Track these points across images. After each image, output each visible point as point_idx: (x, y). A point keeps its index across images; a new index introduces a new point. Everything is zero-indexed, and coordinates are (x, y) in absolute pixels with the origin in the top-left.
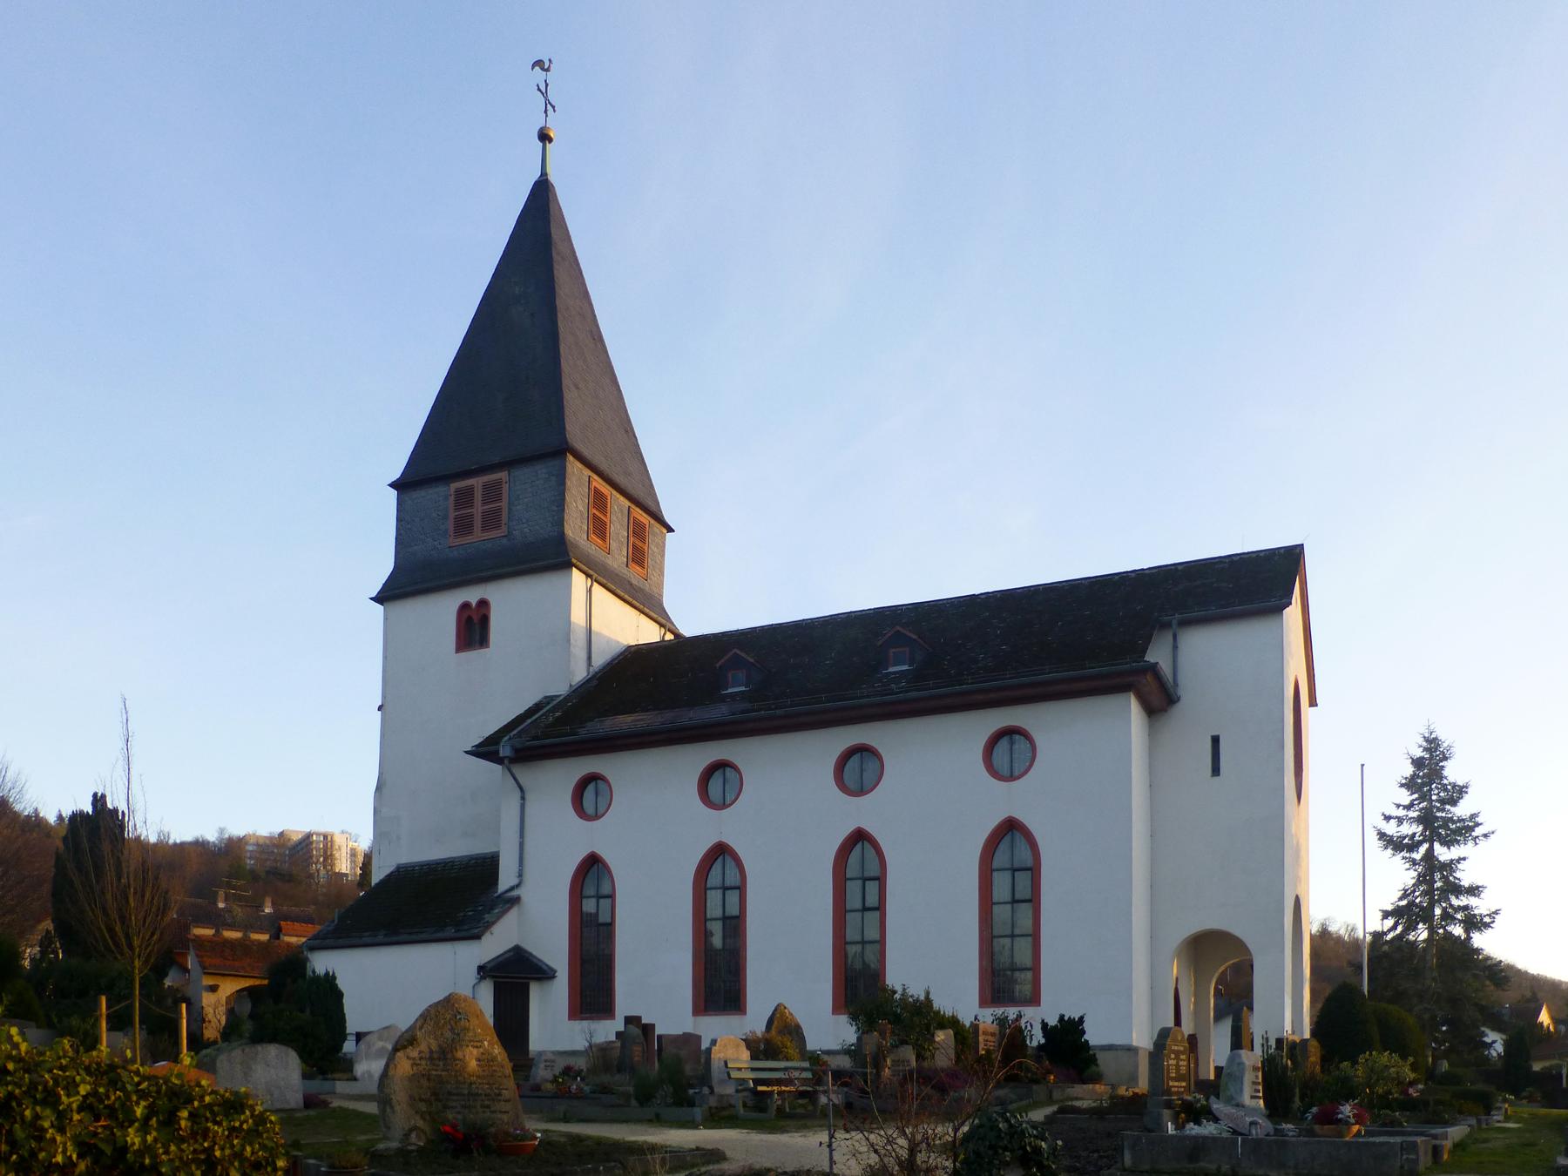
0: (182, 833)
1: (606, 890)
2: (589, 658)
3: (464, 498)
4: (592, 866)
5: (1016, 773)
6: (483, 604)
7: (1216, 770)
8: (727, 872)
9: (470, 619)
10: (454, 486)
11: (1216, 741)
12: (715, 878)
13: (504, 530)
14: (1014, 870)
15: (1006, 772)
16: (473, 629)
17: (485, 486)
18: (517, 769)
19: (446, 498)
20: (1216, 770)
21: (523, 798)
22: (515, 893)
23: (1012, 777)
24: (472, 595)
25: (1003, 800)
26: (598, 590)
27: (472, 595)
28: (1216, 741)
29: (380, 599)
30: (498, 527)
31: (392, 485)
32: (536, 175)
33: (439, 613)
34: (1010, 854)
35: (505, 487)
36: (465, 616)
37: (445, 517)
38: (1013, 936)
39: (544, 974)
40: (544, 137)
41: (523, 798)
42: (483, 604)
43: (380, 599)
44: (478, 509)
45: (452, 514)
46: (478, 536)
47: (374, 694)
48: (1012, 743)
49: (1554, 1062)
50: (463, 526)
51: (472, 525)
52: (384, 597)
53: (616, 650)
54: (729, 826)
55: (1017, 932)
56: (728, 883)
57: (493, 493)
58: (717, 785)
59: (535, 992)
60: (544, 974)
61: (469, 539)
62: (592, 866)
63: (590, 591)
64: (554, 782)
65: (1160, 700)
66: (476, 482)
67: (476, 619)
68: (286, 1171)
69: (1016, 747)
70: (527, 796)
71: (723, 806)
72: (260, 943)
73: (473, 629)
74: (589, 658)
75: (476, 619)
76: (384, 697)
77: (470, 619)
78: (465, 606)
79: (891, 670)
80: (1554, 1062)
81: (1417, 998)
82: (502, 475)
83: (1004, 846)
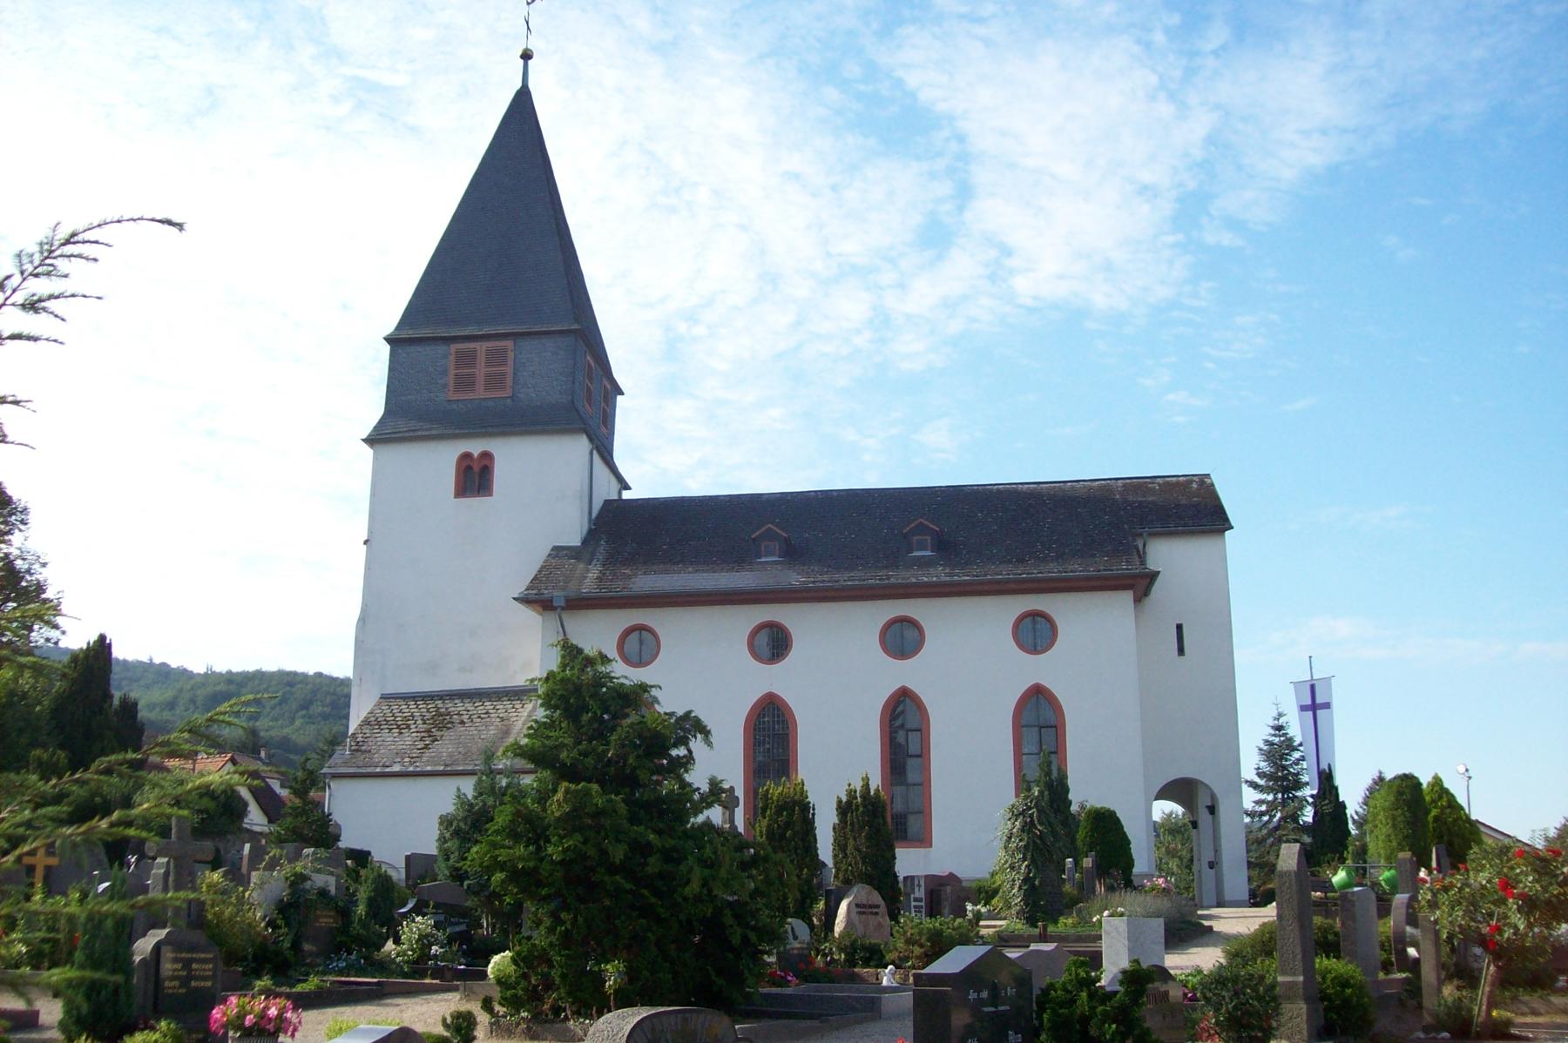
0: (130, 658)
3: (466, 359)
6: (487, 456)
7: (1181, 651)
9: (469, 468)
10: (454, 347)
11: (1179, 627)
13: (508, 392)
16: (474, 478)
17: (489, 352)
18: (565, 616)
19: (445, 356)
20: (1181, 651)
24: (476, 447)
27: (476, 447)
28: (1179, 627)
31: (388, 339)
32: (519, 85)
33: (438, 462)
34: (1039, 718)
35: (511, 355)
37: (445, 373)
40: (527, 56)
42: (487, 456)
43: (371, 441)
44: (481, 370)
45: (453, 372)
46: (480, 393)
47: (360, 528)
48: (1034, 622)
49: (144, 834)
50: (464, 383)
51: (473, 383)
54: (779, 679)
57: (497, 358)
61: (471, 396)
65: (1141, 584)
66: (481, 347)
68: (75, 1023)
73: (474, 478)
75: (476, 469)
76: (370, 531)
77: (469, 468)
78: (466, 456)
80: (144, 834)
82: (509, 344)
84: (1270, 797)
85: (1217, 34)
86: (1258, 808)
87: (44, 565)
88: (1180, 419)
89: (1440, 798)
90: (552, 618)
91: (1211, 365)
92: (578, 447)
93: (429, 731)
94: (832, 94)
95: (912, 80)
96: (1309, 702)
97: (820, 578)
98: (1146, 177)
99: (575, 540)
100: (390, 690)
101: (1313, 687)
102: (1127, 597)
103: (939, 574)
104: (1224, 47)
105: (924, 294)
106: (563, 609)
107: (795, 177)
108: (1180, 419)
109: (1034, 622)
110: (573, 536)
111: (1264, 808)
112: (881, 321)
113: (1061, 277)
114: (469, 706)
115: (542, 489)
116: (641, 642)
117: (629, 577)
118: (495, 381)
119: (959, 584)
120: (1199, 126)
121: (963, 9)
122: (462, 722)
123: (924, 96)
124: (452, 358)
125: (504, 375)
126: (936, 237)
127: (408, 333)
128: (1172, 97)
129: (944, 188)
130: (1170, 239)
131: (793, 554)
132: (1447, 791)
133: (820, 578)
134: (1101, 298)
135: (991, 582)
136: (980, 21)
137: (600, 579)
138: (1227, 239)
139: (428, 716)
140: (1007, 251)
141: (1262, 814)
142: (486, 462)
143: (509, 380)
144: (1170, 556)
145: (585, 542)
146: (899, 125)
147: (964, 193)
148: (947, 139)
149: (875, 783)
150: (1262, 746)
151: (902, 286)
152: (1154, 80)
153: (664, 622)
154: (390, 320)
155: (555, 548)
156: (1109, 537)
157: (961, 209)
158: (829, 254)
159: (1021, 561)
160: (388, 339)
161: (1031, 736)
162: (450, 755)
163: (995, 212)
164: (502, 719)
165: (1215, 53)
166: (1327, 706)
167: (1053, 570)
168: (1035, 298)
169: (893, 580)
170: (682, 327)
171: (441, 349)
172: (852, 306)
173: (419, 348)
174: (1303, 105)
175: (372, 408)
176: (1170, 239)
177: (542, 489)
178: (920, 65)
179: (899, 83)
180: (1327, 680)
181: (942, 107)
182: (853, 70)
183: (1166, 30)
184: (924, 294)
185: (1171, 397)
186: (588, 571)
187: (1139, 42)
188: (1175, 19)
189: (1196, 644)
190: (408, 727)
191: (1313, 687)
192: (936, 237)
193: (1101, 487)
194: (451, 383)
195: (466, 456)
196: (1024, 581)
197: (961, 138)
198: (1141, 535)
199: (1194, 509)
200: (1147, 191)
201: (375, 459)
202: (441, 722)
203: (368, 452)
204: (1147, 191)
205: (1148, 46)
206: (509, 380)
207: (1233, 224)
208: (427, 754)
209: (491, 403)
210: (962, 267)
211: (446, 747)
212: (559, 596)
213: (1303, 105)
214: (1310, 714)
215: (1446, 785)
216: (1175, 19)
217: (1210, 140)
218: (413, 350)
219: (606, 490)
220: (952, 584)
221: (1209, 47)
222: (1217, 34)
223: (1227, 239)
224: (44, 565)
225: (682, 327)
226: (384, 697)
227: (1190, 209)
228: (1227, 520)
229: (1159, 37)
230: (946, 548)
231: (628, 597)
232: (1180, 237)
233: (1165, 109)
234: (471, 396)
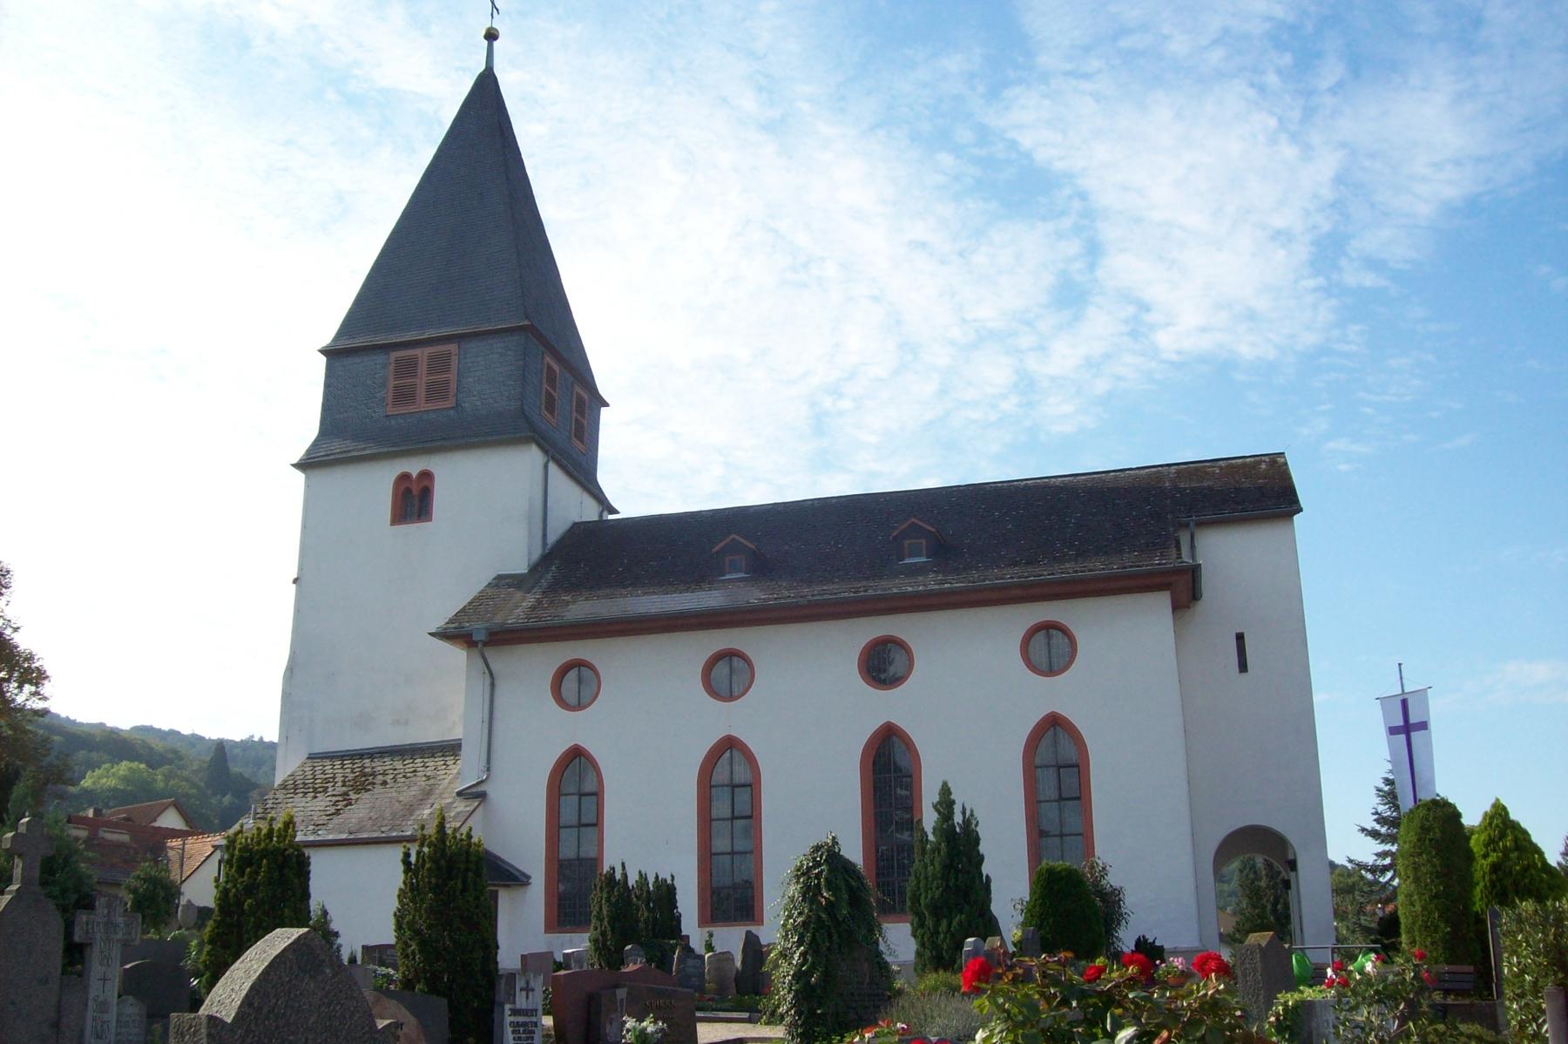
1: (589, 786)
2: (545, 535)
4: (575, 762)
5: (736, 694)
7: (1243, 667)
8: (736, 768)
9: (408, 490)
10: (394, 355)
11: (1240, 637)
12: (721, 774)
14: (1059, 767)
15: (572, 700)
16: (413, 502)
17: (431, 358)
18: (489, 652)
20: (1243, 667)
21: (493, 685)
22: (481, 789)
23: (731, 697)
24: (413, 466)
25: (1046, 695)
26: (553, 467)
27: (413, 466)
28: (1240, 637)
29: (302, 466)
30: (445, 398)
31: (324, 351)
33: (376, 484)
36: (402, 488)
38: (1061, 835)
39: (515, 879)
41: (493, 685)
42: (427, 476)
43: (302, 466)
44: (422, 380)
45: (392, 383)
46: (421, 405)
48: (1049, 637)
50: (404, 395)
52: (306, 465)
53: (567, 526)
55: (1066, 830)
56: (737, 780)
58: (726, 677)
59: (506, 902)
60: (515, 879)
61: (412, 409)
62: (575, 762)
63: (546, 467)
64: (532, 667)
65: (1184, 589)
66: (423, 353)
67: (415, 492)
69: (1054, 641)
70: (497, 682)
71: (579, 706)
72: (119, 845)
73: (413, 502)
74: (545, 535)
75: (415, 492)
76: (301, 569)
79: (907, 561)
81: (1458, 869)
82: (453, 347)
83: (1046, 741)
84: (1394, 848)
85: (1332, 71)
86: (1380, 862)
87: (16, 629)
88: (1343, 467)
89: (1502, 836)
90: (475, 652)
91: (1369, 410)
92: (525, 462)
93: (346, 794)
94: (945, 159)
95: (1026, 141)
96: (1401, 723)
97: (786, 593)
98: (1278, 222)
99: (522, 568)
100: (319, 748)
101: (1404, 703)
102: (1162, 601)
103: (931, 583)
104: (1340, 84)
105: (1065, 356)
106: (486, 644)
107: (922, 245)
108: (1343, 467)
109: (1049, 637)
110: (519, 565)
111: (1388, 861)
112: (1026, 385)
113: (1204, 330)
114: (398, 765)
115: (493, 507)
116: (580, 681)
117: (568, 603)
118: (437, 391)
119: (953, 592)
120: (1326, 165)
121: (1069, 67)
122: (385, 783)
123: (1041, 156)
124: (392, 367)
125: (447, 382)
126: (1070, 297)
127: (342, 344)
128: (1293, 138)
129: (1073, 247)
130: (1311, 283)
131: (761, 568)
132: (1515, 827)
133: (786, 593)
134: (1247, 348)
135: (993, 588)
136: (1086, 76)
137: (533, 608)
138: (1369, 280)
139: (351, 776)
140: (1145, 307)
141: (1385, 869)
142: (425, 483)
143: (453, 386)
144: (1225, 553)
145: (534, 569)
146: (1022, 189)
147: (1094, 251)
148: (1070, 197)
149: (853, 851)
150: (1382, 786)
151: (1042, 349)
152: (1272, 122)
153: (605, 655)
154: (327, 332)
155: (499, 578)
156: (1144, 534)
157: (1092, 267)
158: (964, 320)
159: (1030, 562)
160: (324, 351)
161: (1047, 781)
162: (360, 821)
163: (1127, 267)
164: (428, 778)
165: (1333, 91)
166: (1423, 726)
167: (1068, 570)
168: (1179, 353)
169: (870, 592)
170: (827, 402)
171: (380, 358)
172: (995, 372)
173: (357, 360)
174: (1431, 138)
175: (305, 426)
176: (1311, 283)
177: (493, 507)
178: (1031, 123)
179: (1013, 145)
180: (1422, 693)
181: (1059, 166)
182: (965, 135)
183: (1279, 72)
184: (1065, 356)
185: (1331, 445)
186: (524, 599)
187: (1252, 85)
188: (1287, 59)
189: (1264, 658)
190: (325, 790)
191: (1404, 703)
192: (1070, 297)
193: (1149, 475)
194: (391, 394)
195: (405, 477)
196: (1033, 585)
197: (1083, 196)
198: (1187, 525)
199: (1257, 492)
200: (1281, 237)
201: (307, 486)
202: (362, 783)
203: (300, 477)
204: (1281, 237)
205: (1262, 89)
206: (453, 386)
207: (1374, 264)
208: (336, 820)
209: (432, 415)
210: (1100, 326)
211: (360, 812)
212: (478, 628)
213: (1431, 138)
214: (1403, 737)
215: (1513, 816)
216: (1287, 59)
217: (1339, 180)
218: (348, 361)
219: (572, 507)
220: (942, 593)
221: (1324, 84)
222: (1332, 71)
223: (1369, 280)
224: (16, 629)
225: (827, 402)
226: (312, 757)
227: (1328, 251)
228: (1296, 501)
229: (1272, 79)
230: (944, 553)
231: (561, 627)
232: (1321, 281)
233: (1289, 151)
234: (412, 409)
